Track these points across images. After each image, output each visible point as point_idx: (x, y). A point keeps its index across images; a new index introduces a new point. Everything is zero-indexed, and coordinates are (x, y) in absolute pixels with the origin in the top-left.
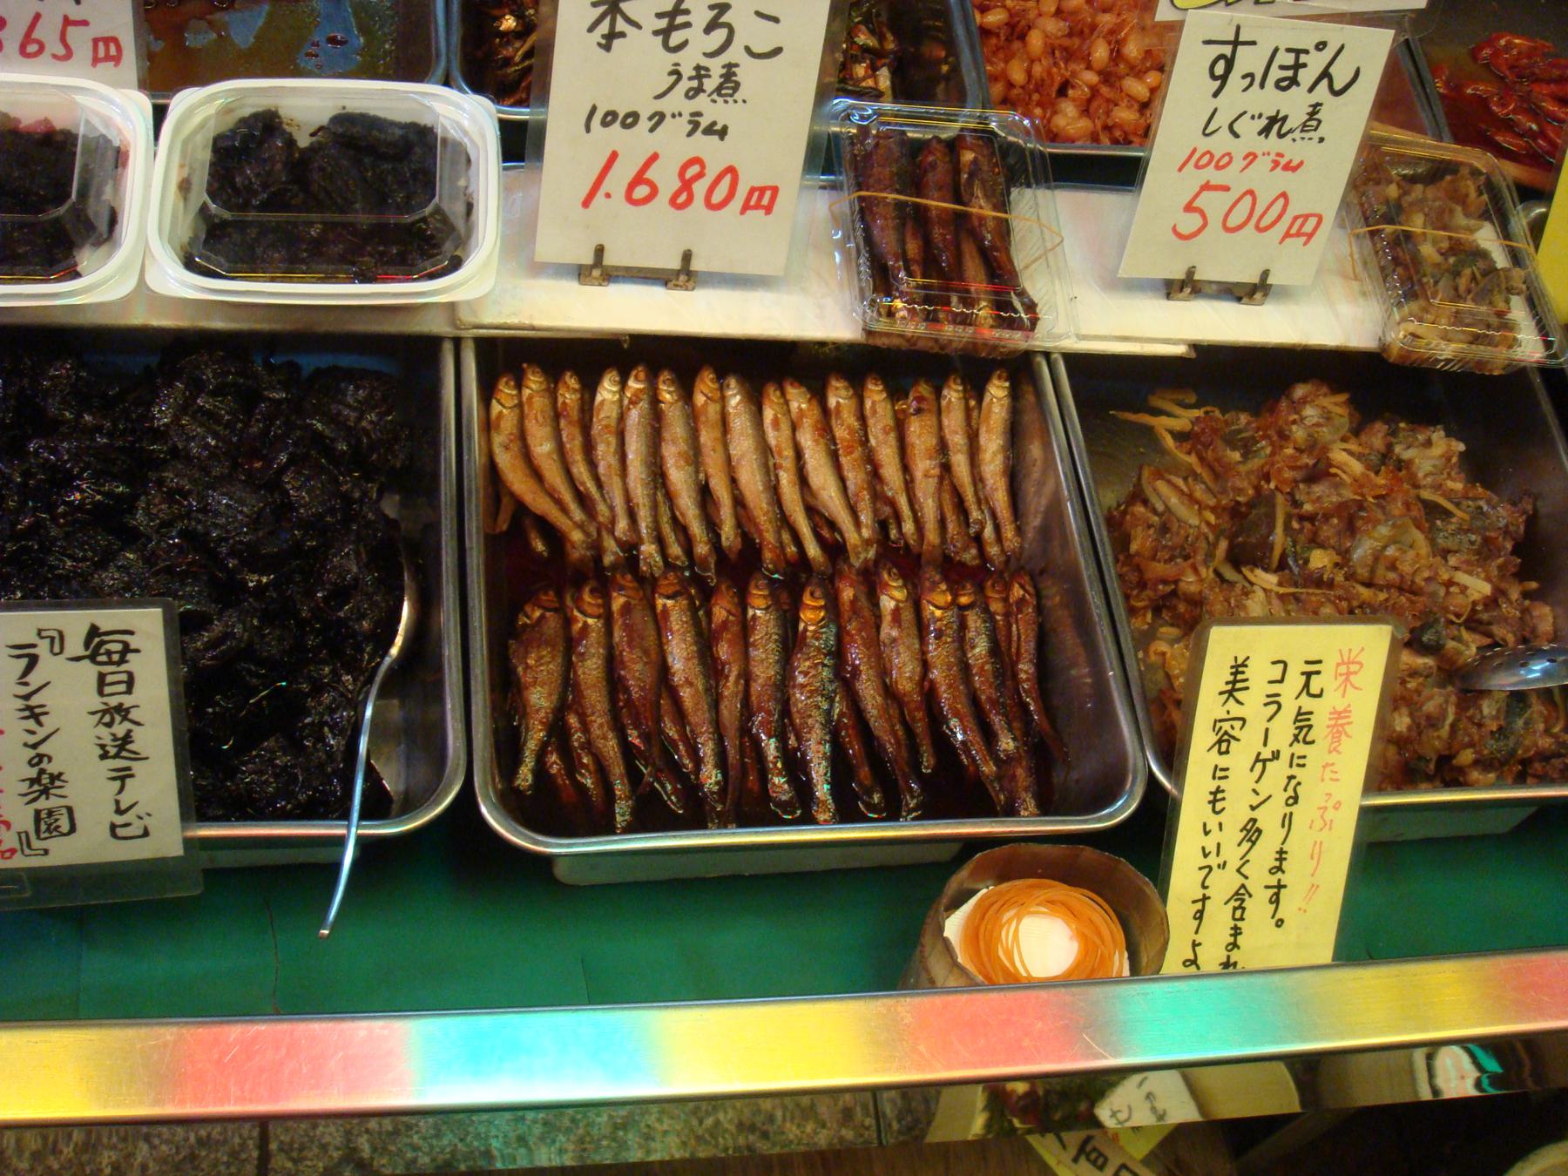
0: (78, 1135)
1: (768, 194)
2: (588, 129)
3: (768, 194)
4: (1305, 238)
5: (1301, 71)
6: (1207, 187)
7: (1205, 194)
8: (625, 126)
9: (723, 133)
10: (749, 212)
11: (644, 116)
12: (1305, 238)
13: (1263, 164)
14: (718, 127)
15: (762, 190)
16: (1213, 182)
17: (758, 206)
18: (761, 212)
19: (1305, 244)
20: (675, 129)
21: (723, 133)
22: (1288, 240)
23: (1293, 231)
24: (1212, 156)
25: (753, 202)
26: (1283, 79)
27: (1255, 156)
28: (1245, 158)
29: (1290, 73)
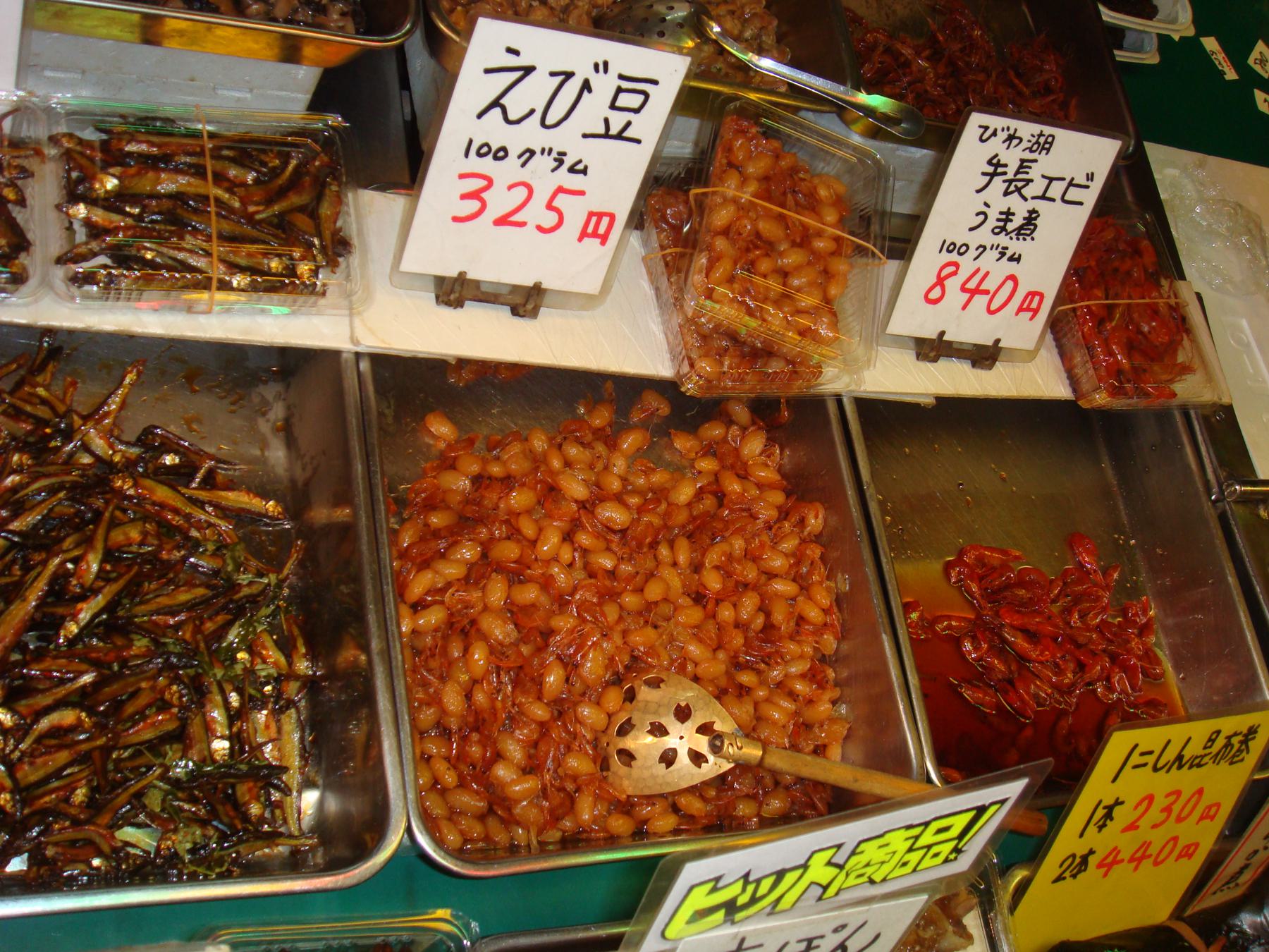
0: (867, 71)
1: (605, 221)
2: (467, 155)
3: (605, 221)
4: (1030, 314)
5: (1009, 224)
6: (560, 190)
7: (561, 196)
8: (496, 158)
9: (1018, 260)
10: (586, 240)
11: (973, 247)
12: (1030, 314)
13: (543, 163)
14: (1016, 256)
15: (600, 215)
16: (566, 186)
17: (595, 234)
18: (598, 241)
19: (1031, 319)
20: (543, 163)
21: (1018, 260)
22: (1021, 314)
23: (1025, 306)
24: (490, 149)
25: (590, 230)
26: (997, 227)
27: (985, 248)
28: (977, 249)
29: (1001, 224)
